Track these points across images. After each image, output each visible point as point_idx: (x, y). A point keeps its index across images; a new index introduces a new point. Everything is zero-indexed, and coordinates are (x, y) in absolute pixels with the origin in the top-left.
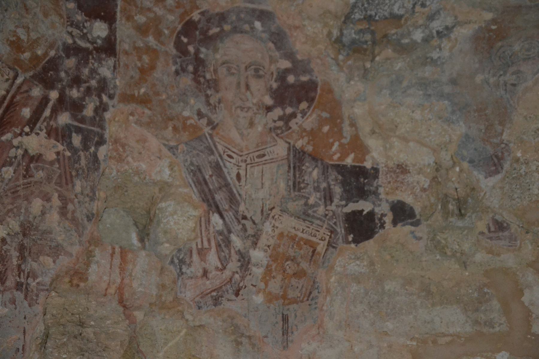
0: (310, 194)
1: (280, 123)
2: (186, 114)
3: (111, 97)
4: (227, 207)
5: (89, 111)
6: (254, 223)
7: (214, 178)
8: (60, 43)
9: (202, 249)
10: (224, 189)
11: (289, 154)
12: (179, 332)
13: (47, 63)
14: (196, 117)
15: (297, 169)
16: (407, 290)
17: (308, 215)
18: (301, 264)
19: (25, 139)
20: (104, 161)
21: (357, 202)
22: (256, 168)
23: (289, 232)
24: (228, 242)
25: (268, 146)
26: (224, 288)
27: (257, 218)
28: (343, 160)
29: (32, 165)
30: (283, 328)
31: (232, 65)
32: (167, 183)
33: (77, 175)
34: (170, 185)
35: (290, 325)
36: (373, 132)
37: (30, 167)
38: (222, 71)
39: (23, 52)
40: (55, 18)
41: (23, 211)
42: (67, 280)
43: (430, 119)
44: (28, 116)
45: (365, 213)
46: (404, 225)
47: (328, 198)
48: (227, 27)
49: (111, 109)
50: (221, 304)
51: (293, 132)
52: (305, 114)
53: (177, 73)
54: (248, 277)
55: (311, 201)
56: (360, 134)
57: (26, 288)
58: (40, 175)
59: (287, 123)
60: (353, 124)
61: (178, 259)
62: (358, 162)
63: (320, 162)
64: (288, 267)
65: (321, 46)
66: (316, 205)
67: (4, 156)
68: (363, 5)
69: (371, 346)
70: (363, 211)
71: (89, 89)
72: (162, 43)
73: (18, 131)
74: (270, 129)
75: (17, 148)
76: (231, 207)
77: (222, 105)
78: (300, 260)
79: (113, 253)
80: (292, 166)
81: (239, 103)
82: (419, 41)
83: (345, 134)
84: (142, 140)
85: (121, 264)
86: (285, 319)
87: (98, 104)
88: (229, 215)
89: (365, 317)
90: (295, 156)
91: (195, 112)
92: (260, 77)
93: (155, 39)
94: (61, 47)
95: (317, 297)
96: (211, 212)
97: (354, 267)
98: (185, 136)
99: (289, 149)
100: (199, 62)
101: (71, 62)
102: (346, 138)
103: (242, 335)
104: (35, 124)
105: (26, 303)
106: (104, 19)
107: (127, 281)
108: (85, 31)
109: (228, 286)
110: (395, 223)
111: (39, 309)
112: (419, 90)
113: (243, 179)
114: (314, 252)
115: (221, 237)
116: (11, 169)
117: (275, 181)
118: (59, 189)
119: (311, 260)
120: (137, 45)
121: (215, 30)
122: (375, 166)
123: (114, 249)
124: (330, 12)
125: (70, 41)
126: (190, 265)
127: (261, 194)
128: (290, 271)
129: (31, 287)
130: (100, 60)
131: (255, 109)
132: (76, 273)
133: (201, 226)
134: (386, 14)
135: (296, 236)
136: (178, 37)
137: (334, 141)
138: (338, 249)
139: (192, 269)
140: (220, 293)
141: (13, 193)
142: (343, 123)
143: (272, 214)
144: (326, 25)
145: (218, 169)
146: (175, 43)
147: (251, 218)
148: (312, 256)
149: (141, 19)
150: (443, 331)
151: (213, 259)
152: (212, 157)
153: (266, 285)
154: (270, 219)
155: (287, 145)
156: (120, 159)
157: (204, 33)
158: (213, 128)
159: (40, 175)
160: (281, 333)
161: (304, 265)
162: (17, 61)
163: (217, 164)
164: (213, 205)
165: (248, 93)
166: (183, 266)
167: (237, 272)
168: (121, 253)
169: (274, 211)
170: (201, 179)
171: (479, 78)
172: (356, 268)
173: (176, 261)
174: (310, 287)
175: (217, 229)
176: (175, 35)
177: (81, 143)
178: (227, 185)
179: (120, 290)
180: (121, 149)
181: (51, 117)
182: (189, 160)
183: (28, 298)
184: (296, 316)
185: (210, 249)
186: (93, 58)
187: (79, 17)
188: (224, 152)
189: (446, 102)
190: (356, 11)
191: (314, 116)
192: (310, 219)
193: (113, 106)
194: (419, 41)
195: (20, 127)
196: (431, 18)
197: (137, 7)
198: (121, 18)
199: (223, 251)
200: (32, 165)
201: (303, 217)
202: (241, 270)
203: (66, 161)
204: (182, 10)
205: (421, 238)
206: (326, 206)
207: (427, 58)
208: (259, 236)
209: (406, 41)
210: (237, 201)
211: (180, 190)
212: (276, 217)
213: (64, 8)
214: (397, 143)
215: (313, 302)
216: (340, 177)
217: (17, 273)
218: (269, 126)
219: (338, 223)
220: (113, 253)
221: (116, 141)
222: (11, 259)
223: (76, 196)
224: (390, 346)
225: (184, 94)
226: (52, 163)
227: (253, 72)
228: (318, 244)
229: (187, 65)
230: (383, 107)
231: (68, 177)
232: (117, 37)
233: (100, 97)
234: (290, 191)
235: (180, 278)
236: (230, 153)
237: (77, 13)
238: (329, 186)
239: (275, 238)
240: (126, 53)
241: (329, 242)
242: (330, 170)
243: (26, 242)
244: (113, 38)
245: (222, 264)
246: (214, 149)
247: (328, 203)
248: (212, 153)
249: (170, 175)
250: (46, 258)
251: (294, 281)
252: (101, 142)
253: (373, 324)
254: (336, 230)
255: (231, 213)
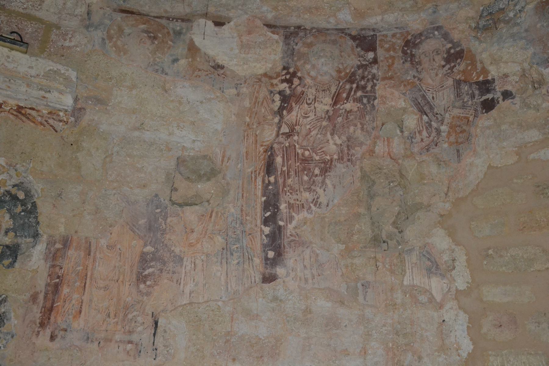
0: (464, 97)
2: (408, 78)
3: (377, 80)
4: (429, 111)
5: (369, 88)
6: (441, 115)
7: (422, 101)
8: (356, 65)
10: (427, 104)
11: (454, 83)
12: (415, 165)
14: (413, 78)
17: (465, 106)
19: (345, 106)
20: (377, 106)
21: (486, 95)
24: (430, 125)
26: (431, 144)
27: (443, 113)
28: (478, 79)
29: (349, 115)
32: (404, 108)
33: (367, 114)
34: (406, 108)
36: (491, 63)
38: (422, 57)
39: (342, 73)
40: (353, 57)
41: (347, 132)
42: (368, 154)
43: (517, 50)
45: (490, 99)
48: (423, 38)
49: (378, 85)
51: (455, 73)
53: (403, 63)
54: (441, 138)
55: (465, 100)
56: (485, 66)
58: (352, 117)
59: (452, 70)
60: (481, 62)
61: (410, 137)
63: (468, 83)
65: (467, 33)
66: (468, 101)
67: (338, 114)
68: (486, 9)
69: (497, 154)
71: (368, 80)
72: (396, 53)
73: (342, 103)
75: (342, 109)
77: (423, 70)
79: (384, 140)
80: (456, 87)
81: (431, 68)
82: (513, 17)
83: (478, 68)
84: (392, 94)
86: (458, 151)
87: (372, 84)
88: (430, 115)
89: (494, 143)
91: (412, 76)
94: (356, 67)
95: (471, 139)
97: (487, 123)
98: (409, 87)
99: (454, 81)
100: (412, 56)
101: (360, 71)
102: (478, 69)
103: (441, 161)
104: (348, 99)
105: (352, 166)
107: (391, 150)
108: (365, 58)
109: (432, 143)
110: (504, 100)
111: (357, 167)
113: (435, 98)
114: (468, 121)
118: (360, 121)
120: (386, 57)
123: (384, 138)
124: (469, 17)
125: (359, 63)
126: (415, 138)
127: (443, 103)
128: (458, 131)
130: (372, 67)
132: (371, 151)
134: (497, 9)
136: (403, 48)
138: (479, 118)
139: (416, 140)
141: (342, 127)
144: (467, 23)
145: (424, 97)
146: (402, 51)
148: (468, 122)
149: (387, 46)
150: (529, 141)
151: (425, 133)
153: (449, 139)
155: (453, 79)
156: (384, 103)
158: (420, 81)
159: (352, 117)
161: (464, 127)
163: (424, 95)
165: (434, 62)
167: (436, 137)
168: (387, 139)
170: (417, 103)
171: (539, 25)
172: (488, 123)
173: (410, 138)
175: (426, 121)
178: (428, 102)
179: (389, 154)
180: (384, 99)
181: (354, 95)
184: (463, 149)
185: (423, 130)
186: (369, 67)
187: (362, 53)
189: (524, 41)
192: (465, 108)
193: (379, 84)
194: (513, 17)
197: (385, 42)
198: (379, 48)
199: (429, 130)
200: (349, 115)
201: (462, 107)
204: (404, 37)
205: (516, 104)
211: (409, 109)
213: (356, 52)
214: (502, 65)
216: (477, 87)
218: (444, 74)
220: (384, 140)
221: (382, 96)
223: (367, 122)
224: (506, 152)
225: (407, 70)
226: (356, 112)
227: (435, 53)
228: (470, 117)
229: (408, 58)
230: (495, 51)
233: (373, 81)
235: (412, 145)
236: (428, 89)
237: (361, 52)
238: (473, 91)
240: (382, 61)
242: (473, 85)
244: (376, 57)
245: (429, 135)
246: (421, 89)
247: (473, 99)
249: (405, 104)
251: (461, 135)
252: (375, 98)
253: (497, 145)
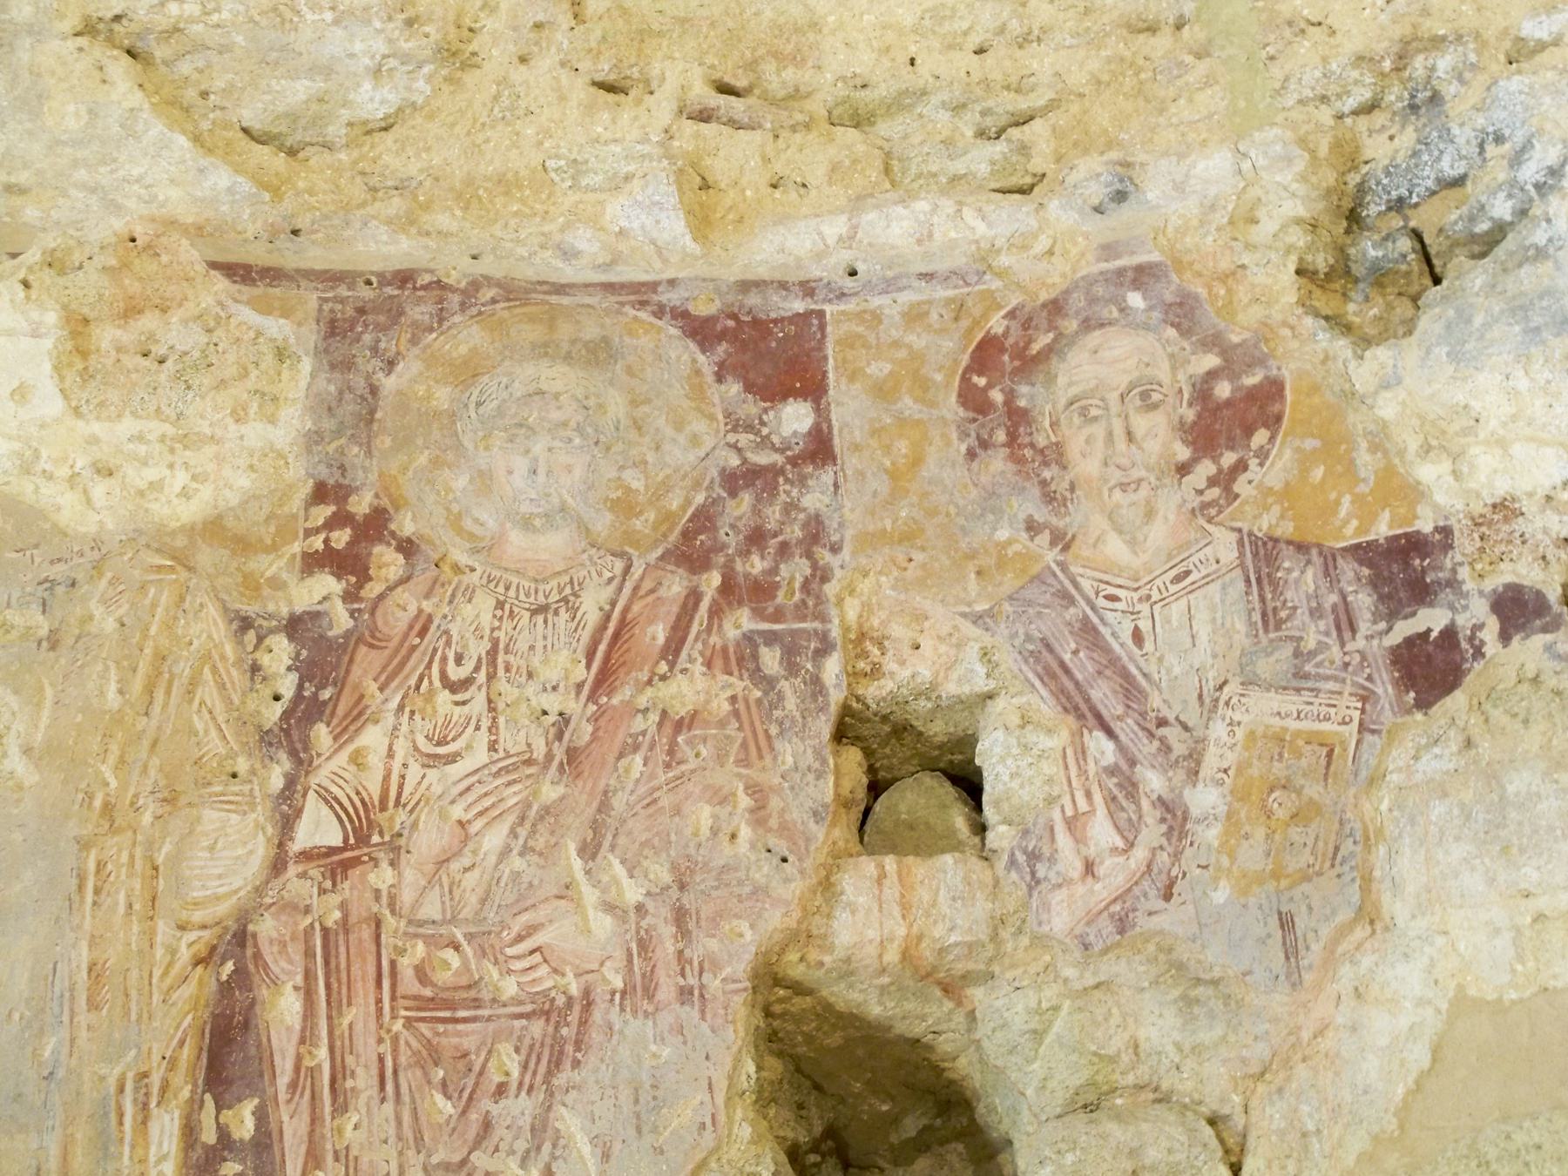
0: (1303, 628)
1: (1215, 492)
2: (1003, 534)
4: (1120, 710)
6: (1186, 728)
7: (1082, 654)
9: (1076, 817)
10: (1108, 672)
11: (1242, 555)
13: (690, 520)
14: (1024, 535)
15: (1265, 582)
16: (1556, 782)
17: (1306, 677)
18: (1306, 791)
19: (665, 691)
21: (1414, 614)
22: (1174, 606)
23: (1267, 727)
24: (1131, 787)
25: (1193, 550)
27: (1192, 718)
30: (1284, 943)
31: (1090, 402)
35: (1299, 933)
37: (677, 744)
44: (661, 640)
45: (1434, 634)
46: (1527, 637)
47: (1344, 625)
49: (838, 573)
50: (1135, 925)
51: (1246, 502)
52: (1267, 457)
53: (971, 455)
54: (1188, 852)
55: (1311, 643)
57: (702, 996)
61: (1025, 852)
62: (1400, 526)
63: (1314, 552)
64: (1276, 805)
70: (1429, 630)
72: (932, 404)
74: (1193, 510)
76: (1129, 707)
78: (1302, 782)
81: (1116, 476)
85: (903, 896)
86: (1286, 923)
87: (808, 571)
88: (1127, 729)
90: (1255, 555)
91: (1022, 526)
92: (1155, 406)
93: (916, 400)
94: (718, 480)
96: (1085, 731)
99: (1240, 543)
100: (1018, 418)
104: (677, 652)
105: (705, 1027)
106: (802, 394)
109: (1146, 884)
110: (1505, 637)
112: (1510, 324)
115: (1115, 780)
116: (638, 759)
117: (1219, 621)
119: (1326, 774)
121: (1043, 340)
122: (1441, 524)
125: (735, 462)
128: (1281, 814)
129: (711, 990)
130: (802, 481)
131: (1152, 479)
133: (1066, 767)
134: (1430, 183)
135: (1285, 730)
136: (965, 379)
137: (1340, 495)
138: (1384, 734)
140: (1128, 905)
142: (1353, 449)
143: (1224, 697)
145: (1088, 632)
146: (960, 395)
147: (1177, 719)
149: (879, 369)
151: (1102, 833)
152: (1072, 610)
153: (1232, 857)
154: (1220, 712)
157: (1020, 353)
158: (1066, 548)
160: (1282, 955)
161: (1313, 790)
162: (630, 537)
163: (1086, 621)
164: (1089, 715)
166: (1038, 866)
167: (1161, 848)
169: (1226, 689)
170: (1055, 666)
172: (1436, 764)
173: (1021, 858)
174: (1333, 837)
175: (1104, 763)
176: (958, 378)
177: (781, 663)
178: (1114, 661)
181: (709, 630)
182: (1021, 631)
183: (709, 1016)
184: (1310, 908)
185: (1093, 812)
186: (787, 480)
188: (1097, 593)
190: (1368, 198)
191: (1288, 454)
192: (1310, 684)
195: (646, 668)
196: (1517, 160)
198: (837, 381)
200: (680, 739)
201: (1295, 683)
202: (1168, 840)
203: (754, 709)
206: (1343, 645)
207: (1528, 249)
208: (1201, 754)
209: (1483, 227)
210: (1141, 691)
212: (1234, 700)
215: (1346, 868)
216: (1366, 571)
217: (678, 969)
219: (1376, 676)
222: (662, 943)
226: (722, 724)
231: (763, 742)
232: (834, 422)
234: (1256, 636)
235: (1035, 894)
236: (1111, 590)
238: (1344, 597)
239: (1239, 748)
241: (1361, 724)
242: (1340, 561)
243: (688, 900)
244: (825, 426)
247: (1347, 635)
248: (1072, 601)
250: (735, 922)
251: (1295, 833)
254: (1373, 693)
255: (1130, 721)
